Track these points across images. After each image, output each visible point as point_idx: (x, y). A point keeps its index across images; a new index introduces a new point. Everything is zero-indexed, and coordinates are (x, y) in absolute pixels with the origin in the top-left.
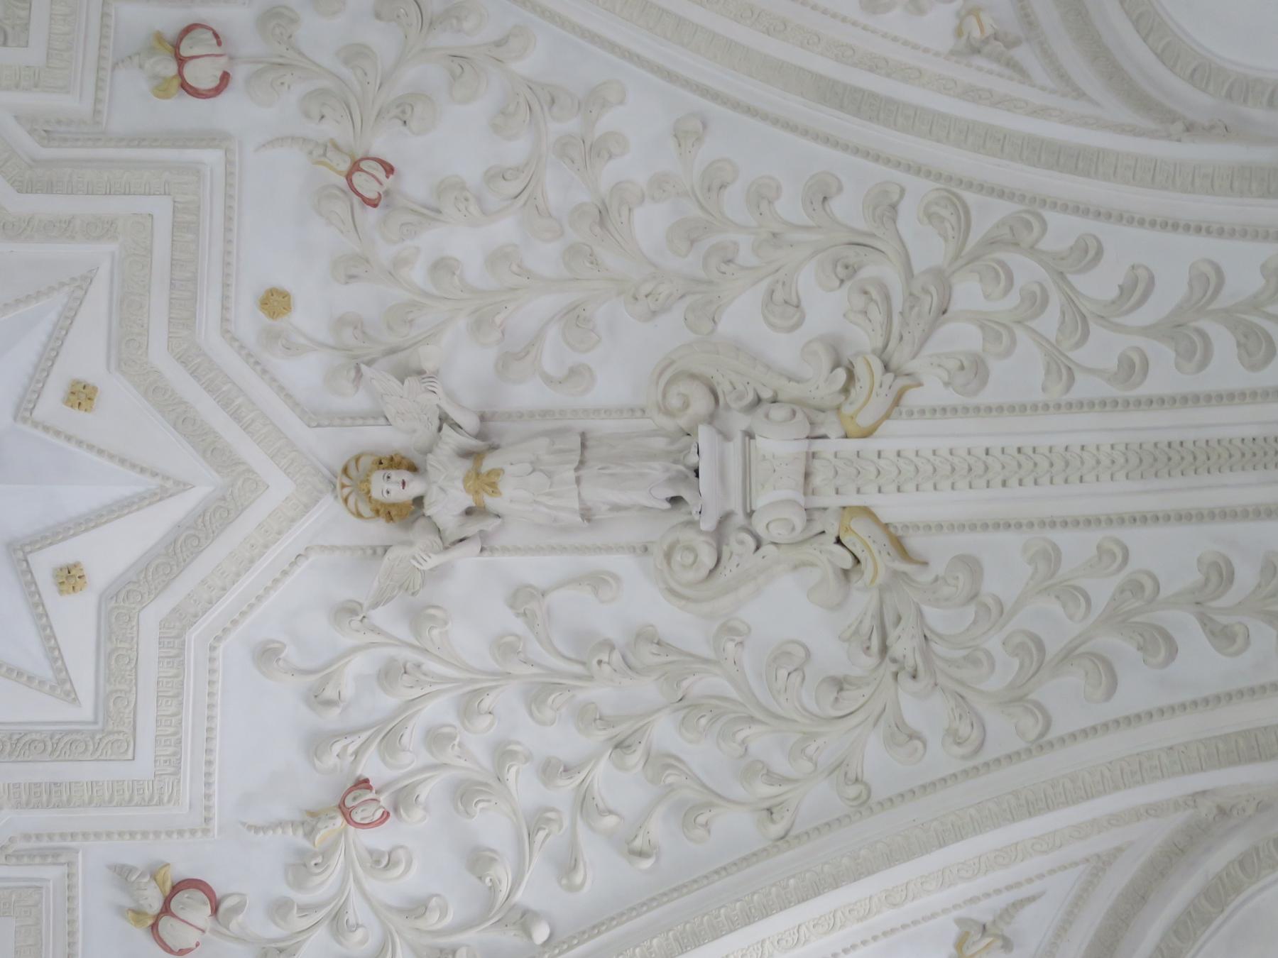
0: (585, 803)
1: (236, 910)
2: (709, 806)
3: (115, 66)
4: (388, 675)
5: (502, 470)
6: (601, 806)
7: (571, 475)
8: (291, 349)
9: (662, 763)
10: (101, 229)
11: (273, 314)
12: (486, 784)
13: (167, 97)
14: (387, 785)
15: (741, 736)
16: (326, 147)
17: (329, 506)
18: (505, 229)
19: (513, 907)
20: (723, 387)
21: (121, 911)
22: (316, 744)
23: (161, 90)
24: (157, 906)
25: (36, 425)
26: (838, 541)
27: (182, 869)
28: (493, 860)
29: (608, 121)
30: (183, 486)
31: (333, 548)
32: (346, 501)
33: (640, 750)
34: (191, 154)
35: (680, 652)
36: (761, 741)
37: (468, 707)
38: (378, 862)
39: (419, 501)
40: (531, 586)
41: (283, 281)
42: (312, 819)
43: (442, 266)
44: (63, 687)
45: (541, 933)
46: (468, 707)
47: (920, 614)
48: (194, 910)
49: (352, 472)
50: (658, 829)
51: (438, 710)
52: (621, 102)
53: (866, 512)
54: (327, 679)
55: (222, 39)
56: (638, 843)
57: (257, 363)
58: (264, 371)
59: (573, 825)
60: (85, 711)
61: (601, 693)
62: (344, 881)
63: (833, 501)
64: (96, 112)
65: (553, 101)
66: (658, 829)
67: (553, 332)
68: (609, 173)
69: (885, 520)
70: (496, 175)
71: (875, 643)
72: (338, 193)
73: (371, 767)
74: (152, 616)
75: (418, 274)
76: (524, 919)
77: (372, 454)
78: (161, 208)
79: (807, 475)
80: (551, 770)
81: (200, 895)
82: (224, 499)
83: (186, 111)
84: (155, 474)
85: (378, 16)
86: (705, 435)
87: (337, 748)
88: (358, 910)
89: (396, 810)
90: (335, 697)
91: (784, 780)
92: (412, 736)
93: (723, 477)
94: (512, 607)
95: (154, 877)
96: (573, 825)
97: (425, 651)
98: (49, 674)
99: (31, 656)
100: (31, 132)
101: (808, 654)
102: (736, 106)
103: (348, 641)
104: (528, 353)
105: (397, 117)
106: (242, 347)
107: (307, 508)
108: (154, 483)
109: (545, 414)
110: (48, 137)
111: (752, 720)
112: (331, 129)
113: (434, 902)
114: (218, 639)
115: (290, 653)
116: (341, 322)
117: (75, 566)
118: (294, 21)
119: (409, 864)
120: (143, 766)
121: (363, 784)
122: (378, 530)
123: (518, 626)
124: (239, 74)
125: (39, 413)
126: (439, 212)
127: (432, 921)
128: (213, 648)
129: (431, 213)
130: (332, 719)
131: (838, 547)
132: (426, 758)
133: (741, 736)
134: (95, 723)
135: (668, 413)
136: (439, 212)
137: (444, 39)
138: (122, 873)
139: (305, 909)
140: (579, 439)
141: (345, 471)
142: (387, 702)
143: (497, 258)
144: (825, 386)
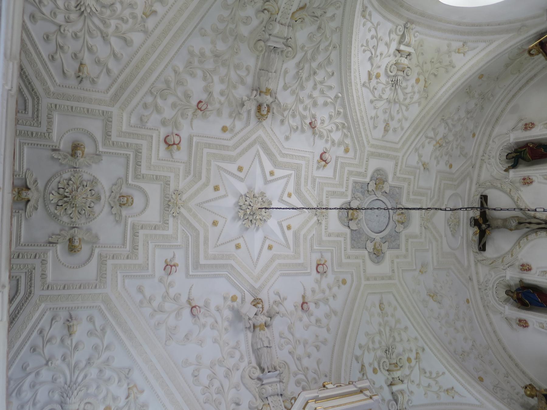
0: (321, 83)
1: (326, 149)
2: (329, 59)
3: (173, 158)
4: (294, 116)
5: (266, 88)
6: (323, 80)
7: (270, 73)
8: (234, 127)
9: (320, 66)
10: (209, 163)
11: (227, 130)
12: (314, 101)
13: (180, 148)
14: (311, 119)
15: (321, 50)
16: (194, 115)
17: (264, 123)
18: (216, 79)
19: (334, 99)
20: (259, 38)
21: (323, 169)
22: (303, 131)
23: (179, 149)
24: (175, 146)
25: (245, 178)
26: (296, 21)
27: (318, 158)
28: (326, 101)
29: (197, 51)
30: (258, 151)
31: (271, 123)
32: (264, 120)
33: (317, 70)
34: (194, 144)
35: (302, 58)
36: (322, 47)
37: (302, 102)
38: (323, 123)
39: (268, 105)
40: (283, 86)
41: (220, 127)
42: (314, 133)
43: (222, 93)
44: (289, 176)
45: (340, 95)
46: (302, 102)
47: (314, 8)
48: (326, 156)
49: (259, 118)
50: (329, 70)
51: (301, 108)
52: (193, 47)
53: (293, 13)
54: (293, 128)
55: (168, 135)
56: (331, 74)
57: (236, 134)
58: (238, 133)
59: (324, 85)
60: (293, 172)
61: (304, 75)
62: (325, 129)
63: (289, 20)
64: (184, 163)
65: (191, 63)
66: (329, 70)
67: (238, 72)
68: (208, 53)
69: (296, 10)
70: (205, 78)
71: (316, 19)
72: (204, 113)
73: (308, 121)
74: (280, 159)
75: (223, 99)
76: (337, 97)
77: (256, 113)
78: (206, 151)
79: (282, 24)
80: (315, 87)
81: (167, 138)
82: (261, 143)
83: (184, 145)
84: (255, 156)
85: (166, 99)
86: (269, 44)
87: (304, 127)
88: (329, 128)
89: (315, 118)
90: (296, 127)
91: (330, 43)
92: (304, 113)
93: (276, 42)
94: (286, 90)
95: (319, 163)
96: (324, 85)
97: (291, 108)
98: (286, 178)
99: (284, 181)
100: (188, 176)
101: (311, 33)
102: (201, 20)
103: (287, 123)
104: (242, 78)
105: (189, 98)
106: (233, 137)
107: (264, 127)
108: (257, 157)
109: (254, 76)
110: (189, 173)
111: (318, 47)
112: (190, 113)
113: (330, 114)
114: (284, 147)
115: (287, 134)
116: (230, 116)
117: (270, 172)
118: (165, 118)
119: (324, 117)
120: (303, 162)
121: (310, 123)
122: (270, 115)
123: (290, 89)
124: (176, 132)
125: (243, 178)
126: (210, 92)
127: (333, 114)
128: (285, 148)
129: (210, 94)
130: (300, 127)
131: (297, 22)
132: (308, 111)
133: (321, 50)
134: (295, 171)
135: (262, 51)
136: (210, 92)
137: (172, 85)
138: (318, 168)
139: (328, 137)
140: (262, 71)
141: (259, 119)
142: (298, 117)
143: (222, 81)
144: (265, 16)
